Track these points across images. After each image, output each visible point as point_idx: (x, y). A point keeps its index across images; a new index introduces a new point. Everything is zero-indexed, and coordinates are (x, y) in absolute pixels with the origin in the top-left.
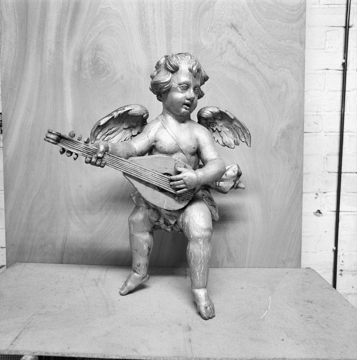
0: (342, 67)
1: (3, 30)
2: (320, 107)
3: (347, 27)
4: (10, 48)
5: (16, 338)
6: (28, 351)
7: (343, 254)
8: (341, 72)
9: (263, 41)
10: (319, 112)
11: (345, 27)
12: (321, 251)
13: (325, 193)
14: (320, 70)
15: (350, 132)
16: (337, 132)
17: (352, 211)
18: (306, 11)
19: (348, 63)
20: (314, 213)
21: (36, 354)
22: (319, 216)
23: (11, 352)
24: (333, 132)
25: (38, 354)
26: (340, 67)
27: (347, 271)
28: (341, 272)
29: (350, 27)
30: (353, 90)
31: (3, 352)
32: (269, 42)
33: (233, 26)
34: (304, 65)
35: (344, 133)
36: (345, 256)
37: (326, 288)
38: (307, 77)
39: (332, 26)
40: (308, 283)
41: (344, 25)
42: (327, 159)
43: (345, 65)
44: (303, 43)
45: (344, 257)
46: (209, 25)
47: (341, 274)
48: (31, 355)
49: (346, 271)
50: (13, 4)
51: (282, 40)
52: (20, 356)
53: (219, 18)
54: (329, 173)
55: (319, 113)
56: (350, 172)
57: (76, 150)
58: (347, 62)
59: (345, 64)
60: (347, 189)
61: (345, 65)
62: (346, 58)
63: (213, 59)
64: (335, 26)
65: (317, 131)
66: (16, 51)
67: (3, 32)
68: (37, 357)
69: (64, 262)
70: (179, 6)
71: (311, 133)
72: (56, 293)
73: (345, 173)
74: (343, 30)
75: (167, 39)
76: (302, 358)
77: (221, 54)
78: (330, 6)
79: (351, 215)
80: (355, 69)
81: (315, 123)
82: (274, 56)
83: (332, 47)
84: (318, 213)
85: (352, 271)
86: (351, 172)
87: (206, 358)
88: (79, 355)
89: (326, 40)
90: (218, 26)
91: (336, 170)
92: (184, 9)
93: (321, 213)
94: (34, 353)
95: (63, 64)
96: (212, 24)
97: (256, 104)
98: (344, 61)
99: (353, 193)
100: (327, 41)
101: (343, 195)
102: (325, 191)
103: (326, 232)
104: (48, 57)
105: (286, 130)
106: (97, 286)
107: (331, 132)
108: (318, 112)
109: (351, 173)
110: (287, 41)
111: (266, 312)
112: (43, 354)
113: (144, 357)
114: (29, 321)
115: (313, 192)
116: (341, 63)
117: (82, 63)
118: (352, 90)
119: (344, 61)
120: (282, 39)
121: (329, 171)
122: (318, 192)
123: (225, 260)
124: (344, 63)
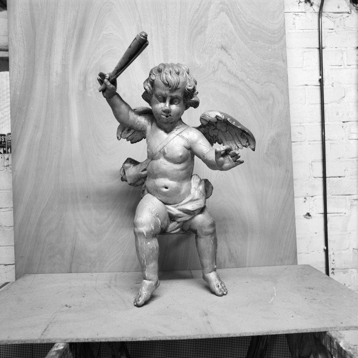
0: (319, 82)
1: (12, 55)
2: (303, 119)
3: (321, 48)
4: (19, 71)
5: (45, 330)
6: (60, 339)
7: (333, 254)
8: (319, 88)
9: (250, 60)
10: (302, 123)
11: (319, 48)
12: (313, 251)
13: (312, 197)
14: (300, 86)
15: (331, 140)
16: (319, 141)
17: (338, 212)
18: (285, 34)
19: (324, 79)
20: (304, 216)
21: (67, 341)
22: (309, 218)
23: (44, 341)
24: (316, 140)
25: (69, 341)
26: (317, 83)
27: (338, 269)
28: (332, 271)
29: (323, 48)
30: (331, 103)
31: (35, 341)
32: (255, 60)
33: (223, 48)
34: (287, 80)
35: (326, 142)
36: (335, 254)
37: (324, 278)
38: (290, 92)
39: (307, 48)
40: (306, 275)
41: (318, 46)
42: (312, 165)
43: (321, 81)
44: (285, 61)
45: (334, 256)
46: (202, 47)
47: (333, 273)
48: (62, 342)
49: (337, 269)
50: (22, 31)
51: (267, 59)
52: (51, 344)
53: (210, 41)
54: (315, 179)
55: (301, 124)
56: (333, 176)
57: (320, 19)
58: (323, 78)
59: (322, 80)
60: (332, 193)
61: (321, 81)
62: (321, 74)
63: (207, 77)
64: (310, 48)
65: (302, 141)
66: (24, 73)
67: (12, 57)
68: (68, 344)
69: (72, 272)
70: (174, 31)
71: (296, 143)
72: (73, 295)
73: (329, 177)
74: (317, 51)
75: (164, 61)
76: (312, 328)
77: (214, 72)
78: (304, 30)
79: (337, 216)
80: (330, 85)
81: (299, 133)
82: (260, 73)
83: (309, 66)
84: (308, 216)
85: (343, 269)
86: (335, 176)
87: (226, 334)
88: (109, 340)
89: (303, 60)
90: (209, 48)
91: (321, 175)
92: (179, 34)
93: (310, 216)
94: (65, 340)
95: (69, 84)
96: (204, 46)
97: (247, 115)
98: (320, 77)
99: (338, 196)
100: (304, 61)
101: (329, 198)
102: (312, 195)
103: (316, 233)
104: (55, 79)
105: (276, 138)
106: (110, 288)
107: (314, 141)
108: (301, 123)
109: (335, 177)
110: (272, 60)
111: (273, 298)
112: (74, 341)
113: (169, 337)
114: (53, 317)
115: (302, 196)
116: (318, 80)
117: (86, 83)
118: (329, 102)
119: (320, 77)
120: (267, 58)
121: (315, 177)
122: (306, 196)
123: (227, 260)
124: (321, 79)
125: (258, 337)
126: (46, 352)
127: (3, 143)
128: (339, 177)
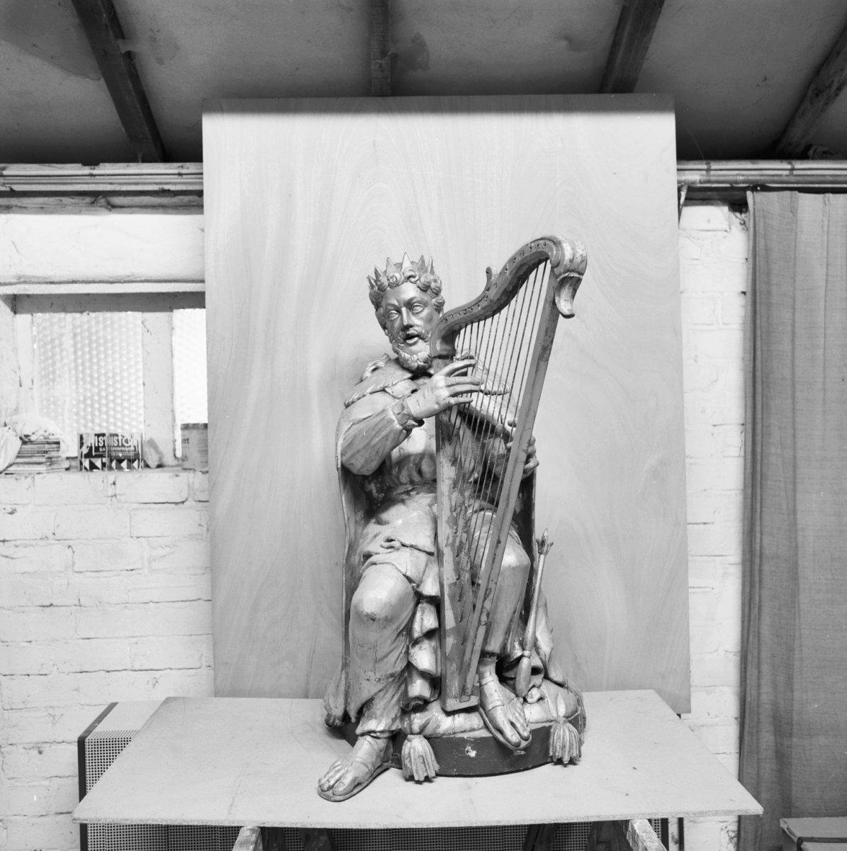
15: (691, 458)
17: (701, 586)
125: (540, 826)
126: (231, 841)
127: (101, 449)
128: (705, 524)
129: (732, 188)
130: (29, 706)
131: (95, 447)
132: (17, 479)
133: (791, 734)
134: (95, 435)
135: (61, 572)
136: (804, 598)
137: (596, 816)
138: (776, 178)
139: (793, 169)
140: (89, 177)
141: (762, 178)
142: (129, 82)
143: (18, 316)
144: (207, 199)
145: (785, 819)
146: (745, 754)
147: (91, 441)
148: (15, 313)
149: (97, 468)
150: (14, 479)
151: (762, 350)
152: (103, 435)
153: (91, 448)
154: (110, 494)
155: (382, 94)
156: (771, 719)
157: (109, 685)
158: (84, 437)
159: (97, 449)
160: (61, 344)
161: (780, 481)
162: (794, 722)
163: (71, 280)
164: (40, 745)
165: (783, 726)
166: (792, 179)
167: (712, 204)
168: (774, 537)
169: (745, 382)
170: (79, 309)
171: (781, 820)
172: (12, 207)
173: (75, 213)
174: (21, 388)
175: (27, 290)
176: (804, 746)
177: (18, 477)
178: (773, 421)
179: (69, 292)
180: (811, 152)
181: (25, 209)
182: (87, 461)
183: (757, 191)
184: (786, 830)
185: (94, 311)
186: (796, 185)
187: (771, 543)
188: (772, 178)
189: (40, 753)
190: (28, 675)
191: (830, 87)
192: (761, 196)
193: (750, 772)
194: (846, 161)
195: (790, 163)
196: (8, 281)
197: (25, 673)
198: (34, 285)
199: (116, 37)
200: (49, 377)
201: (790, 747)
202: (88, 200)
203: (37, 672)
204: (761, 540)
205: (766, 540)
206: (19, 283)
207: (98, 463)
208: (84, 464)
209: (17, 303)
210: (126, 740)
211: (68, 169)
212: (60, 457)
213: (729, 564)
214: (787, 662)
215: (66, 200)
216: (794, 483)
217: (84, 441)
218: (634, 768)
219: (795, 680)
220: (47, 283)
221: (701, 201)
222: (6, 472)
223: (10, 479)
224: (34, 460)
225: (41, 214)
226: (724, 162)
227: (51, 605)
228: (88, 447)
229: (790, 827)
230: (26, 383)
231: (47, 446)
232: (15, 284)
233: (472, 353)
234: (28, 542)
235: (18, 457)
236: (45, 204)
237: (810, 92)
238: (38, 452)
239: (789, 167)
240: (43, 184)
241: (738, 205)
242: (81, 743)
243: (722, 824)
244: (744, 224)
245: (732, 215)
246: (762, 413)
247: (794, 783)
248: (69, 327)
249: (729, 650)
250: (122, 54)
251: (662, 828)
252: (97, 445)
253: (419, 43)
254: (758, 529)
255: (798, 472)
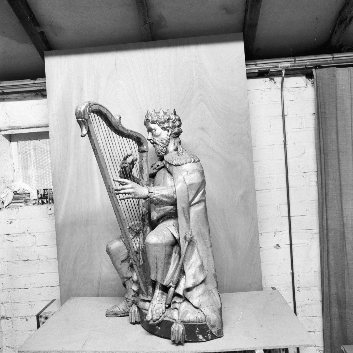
127: (46, 195)
128: (302, 216)
129: (306, 68)
130: (21, 301)
131: (43, 195)
132: (12, 209)
133: (345, 308)
134: (43, 190)
135: (32, 246)
136: (348, 247)
137: (239, 349)
138: (325, 62)
139: (333, 58)
140: (33, 84)
141: (319, 62)
142: (43, 44)
143: (12, 143)
144: (48, 93)
145: (343, 346)
146: (325, 317)
147: (42, 192)
148: (11, 142)
149: (45, 203)
150: (11, 209)
151: (323, 138)
152: (47, 189)
153: (42, 195)
154: (49, 214)
155: (147, 40)
156: (336, 301)
157: (52, 292)
158: (39, 191)
159: (44, 195)
160: (30, 153)
161: (334, 196)
162: (346, 302)
163: (30, 127)
164: (26, 317)
165: (342, 304)
166: (333, 62)
167: (298, 76)
168: (333, 220)
169: (316, 153)
170: (36, 139)
171: (341, 346)
172: (5, 99)
173: (29, 100)
174: (14, 172)
175: (14, 132)
176: (351, 313)
177: (12, 208)
178: (330, 170)
179: (30, 132)
180: (343, 49)
181: (10, 99)
182: (41, 200)
183: (317, 68)
184: (343, 350)
185: (42, 139)
186: (335, 65)
187: (333, 224)
188: (323, 62)
189: (27, 320)
190: (21, 289)
191: (346, 19)
192: (319, 71)
193: (327, 325)
194: (352, 51)
195: (332, 55)
196: (5, 129)
197: (18, 288)
198: (16, 130)
199: (35, 26)
200: (26, 167)
201: (345, 313)
202: (34, 94)
203: (23, 287)
204: (327, 222)
205: (330, 222)
206: (10, 129)
207: (45, 201)
208: (39, 202)
209: (11, 138)
210: (49, 315)
211: (24, 82)
212: (30, 199)
213: (314, 233)
214: (342, 276)
215: (25, 95)
216: (341, 197)
217: (39, 192)
218: (261, 326)
219: (346, 284)
220: (21, 129)
221: (293, 75)
222: (8, 206)
223: (9, 209)
224: (19, 201)
225: (16, 101)
226: (302, 57)
227: (28, 260)
228: (40, 195)
229: (346, 349)
230: (16, 170)
231: (24, 195)
232: (9, 130)
233: (129, 153)
234: (17, 235)
235: (13, 200)
236: (17, 97)
237: (338, 22)
238: (21, 198)
239: (332, 57)
240: (14, 88)
241: (309, 76)
242: (38, 316)
243: (317, 348)
244: (313, 83)
245: (308, 80)
246: (325, 166)
247: (348, 329)
248: (32, 147)
249: (316, 271)
250: (38, 32)
251: (285, 352)
252: (44, 194)
253: (162, 18)
254: (325, 217)
255: (343, 191)
